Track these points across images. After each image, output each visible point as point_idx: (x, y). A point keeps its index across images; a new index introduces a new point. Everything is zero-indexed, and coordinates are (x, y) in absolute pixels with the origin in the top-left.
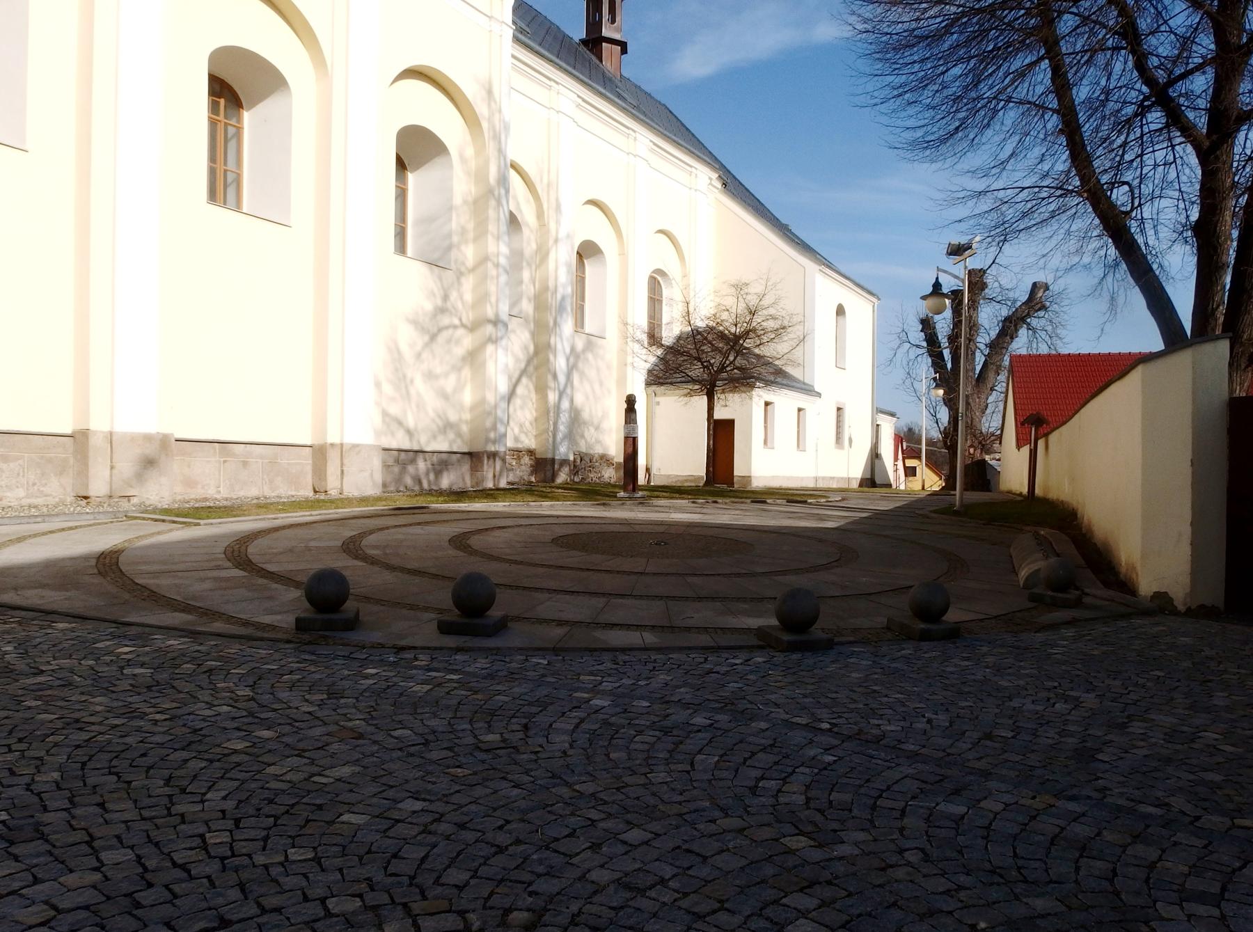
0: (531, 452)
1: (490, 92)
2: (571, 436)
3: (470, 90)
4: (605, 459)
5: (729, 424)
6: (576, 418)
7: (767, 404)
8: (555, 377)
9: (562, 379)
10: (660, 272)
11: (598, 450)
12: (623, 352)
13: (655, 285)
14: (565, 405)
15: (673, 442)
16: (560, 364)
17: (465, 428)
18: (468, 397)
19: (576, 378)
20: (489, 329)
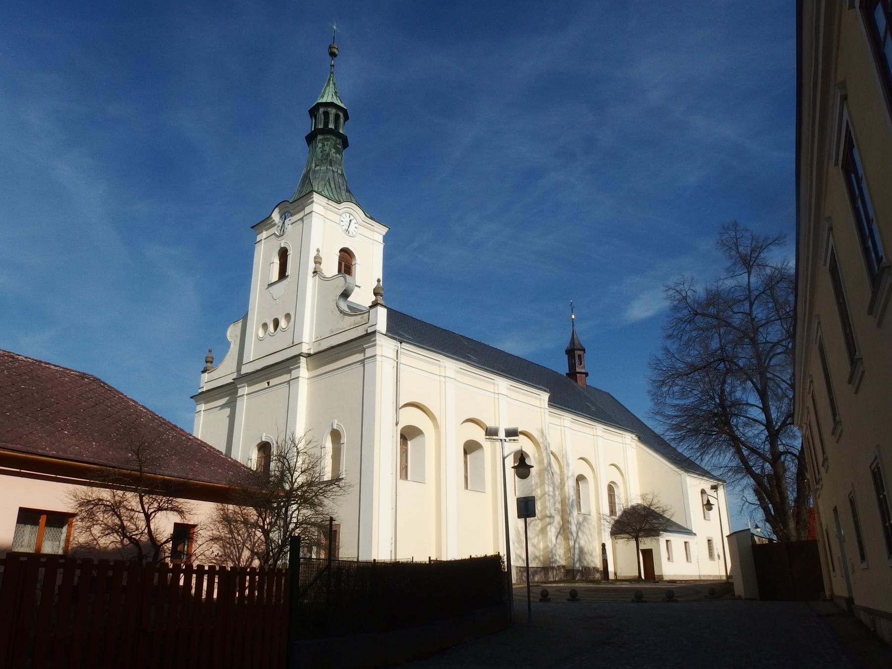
0: (564, 567)
1: (542, 433)
2: (580, 560)
3: (535, 434)
4: (596, 569)
5: (651, 551)
6: (581, 550)
7: (667, 541)
8: (572, 534)
9: (575, 535)
10: (613, 482)
11: (592, 565)
12: (600, 525)
13: (611, 489)
14: (577, 546)
15: (623, 560)
16: (574, 528)
17: (542, 558)
18: (541, 546)
19: (580, 534)
20: (548, 520)
